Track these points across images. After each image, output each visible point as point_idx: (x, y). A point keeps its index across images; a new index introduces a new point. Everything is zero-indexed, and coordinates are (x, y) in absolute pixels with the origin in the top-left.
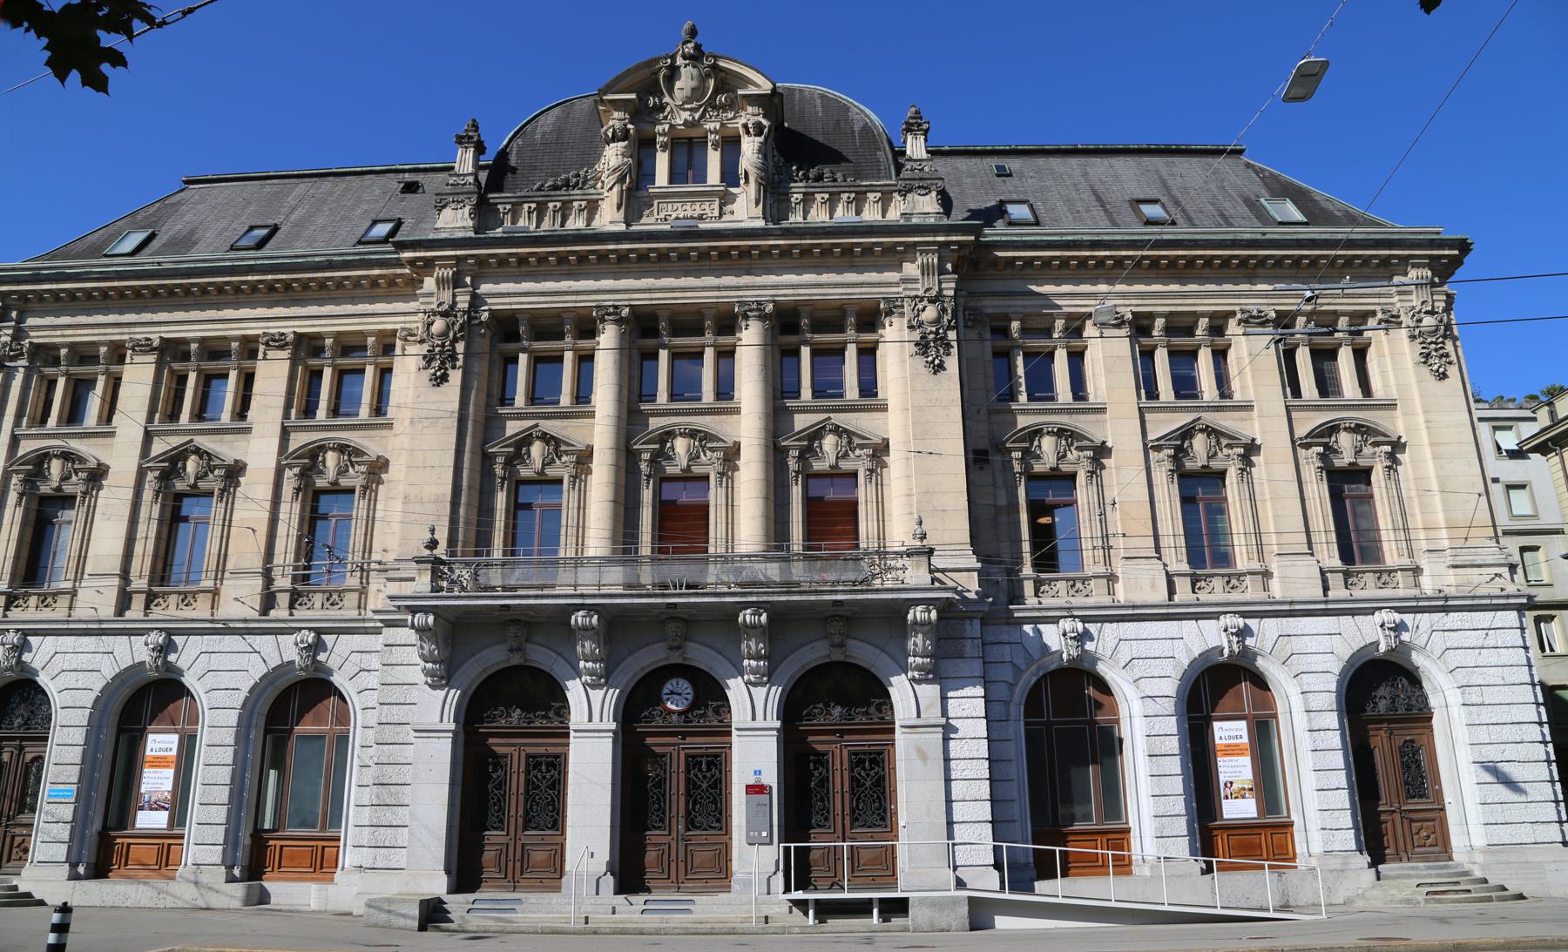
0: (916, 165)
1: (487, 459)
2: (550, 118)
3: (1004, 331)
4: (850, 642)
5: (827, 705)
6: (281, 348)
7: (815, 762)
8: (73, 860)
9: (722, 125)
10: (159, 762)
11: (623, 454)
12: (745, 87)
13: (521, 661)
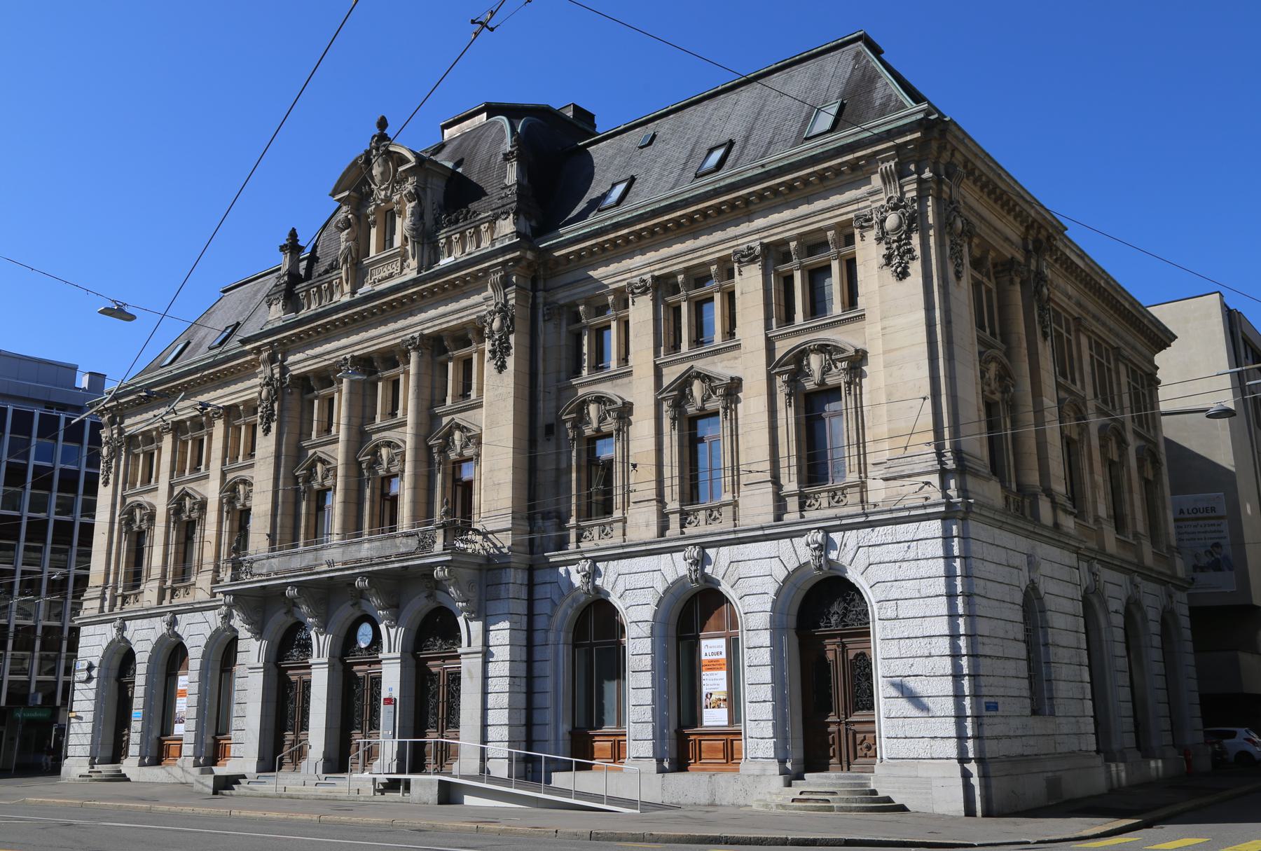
3: (577, 317)
6: (752, 261)
8: (781, 757)
10: (714, 665)
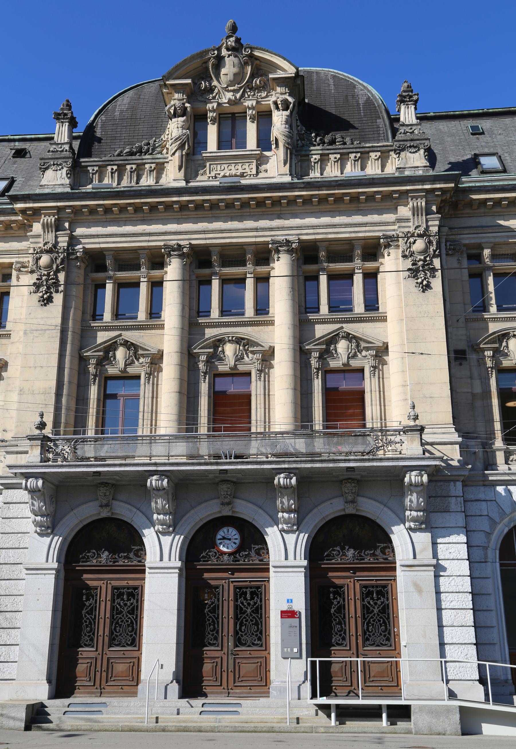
0: (408, 129)
1: (83, 361)
2: (126, 99)
3: (478, 257)
4: (360, 499)
5: (343, 548)
7: (335, 593)
9: (258, 102)
11: (186, 357)
12: (275, 72)
13: (109, 515)
